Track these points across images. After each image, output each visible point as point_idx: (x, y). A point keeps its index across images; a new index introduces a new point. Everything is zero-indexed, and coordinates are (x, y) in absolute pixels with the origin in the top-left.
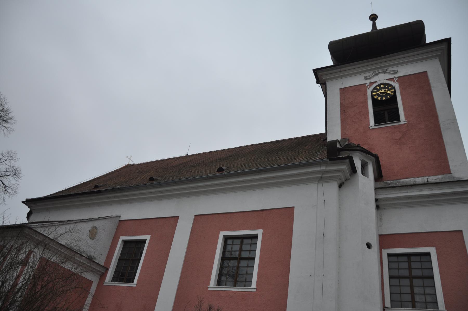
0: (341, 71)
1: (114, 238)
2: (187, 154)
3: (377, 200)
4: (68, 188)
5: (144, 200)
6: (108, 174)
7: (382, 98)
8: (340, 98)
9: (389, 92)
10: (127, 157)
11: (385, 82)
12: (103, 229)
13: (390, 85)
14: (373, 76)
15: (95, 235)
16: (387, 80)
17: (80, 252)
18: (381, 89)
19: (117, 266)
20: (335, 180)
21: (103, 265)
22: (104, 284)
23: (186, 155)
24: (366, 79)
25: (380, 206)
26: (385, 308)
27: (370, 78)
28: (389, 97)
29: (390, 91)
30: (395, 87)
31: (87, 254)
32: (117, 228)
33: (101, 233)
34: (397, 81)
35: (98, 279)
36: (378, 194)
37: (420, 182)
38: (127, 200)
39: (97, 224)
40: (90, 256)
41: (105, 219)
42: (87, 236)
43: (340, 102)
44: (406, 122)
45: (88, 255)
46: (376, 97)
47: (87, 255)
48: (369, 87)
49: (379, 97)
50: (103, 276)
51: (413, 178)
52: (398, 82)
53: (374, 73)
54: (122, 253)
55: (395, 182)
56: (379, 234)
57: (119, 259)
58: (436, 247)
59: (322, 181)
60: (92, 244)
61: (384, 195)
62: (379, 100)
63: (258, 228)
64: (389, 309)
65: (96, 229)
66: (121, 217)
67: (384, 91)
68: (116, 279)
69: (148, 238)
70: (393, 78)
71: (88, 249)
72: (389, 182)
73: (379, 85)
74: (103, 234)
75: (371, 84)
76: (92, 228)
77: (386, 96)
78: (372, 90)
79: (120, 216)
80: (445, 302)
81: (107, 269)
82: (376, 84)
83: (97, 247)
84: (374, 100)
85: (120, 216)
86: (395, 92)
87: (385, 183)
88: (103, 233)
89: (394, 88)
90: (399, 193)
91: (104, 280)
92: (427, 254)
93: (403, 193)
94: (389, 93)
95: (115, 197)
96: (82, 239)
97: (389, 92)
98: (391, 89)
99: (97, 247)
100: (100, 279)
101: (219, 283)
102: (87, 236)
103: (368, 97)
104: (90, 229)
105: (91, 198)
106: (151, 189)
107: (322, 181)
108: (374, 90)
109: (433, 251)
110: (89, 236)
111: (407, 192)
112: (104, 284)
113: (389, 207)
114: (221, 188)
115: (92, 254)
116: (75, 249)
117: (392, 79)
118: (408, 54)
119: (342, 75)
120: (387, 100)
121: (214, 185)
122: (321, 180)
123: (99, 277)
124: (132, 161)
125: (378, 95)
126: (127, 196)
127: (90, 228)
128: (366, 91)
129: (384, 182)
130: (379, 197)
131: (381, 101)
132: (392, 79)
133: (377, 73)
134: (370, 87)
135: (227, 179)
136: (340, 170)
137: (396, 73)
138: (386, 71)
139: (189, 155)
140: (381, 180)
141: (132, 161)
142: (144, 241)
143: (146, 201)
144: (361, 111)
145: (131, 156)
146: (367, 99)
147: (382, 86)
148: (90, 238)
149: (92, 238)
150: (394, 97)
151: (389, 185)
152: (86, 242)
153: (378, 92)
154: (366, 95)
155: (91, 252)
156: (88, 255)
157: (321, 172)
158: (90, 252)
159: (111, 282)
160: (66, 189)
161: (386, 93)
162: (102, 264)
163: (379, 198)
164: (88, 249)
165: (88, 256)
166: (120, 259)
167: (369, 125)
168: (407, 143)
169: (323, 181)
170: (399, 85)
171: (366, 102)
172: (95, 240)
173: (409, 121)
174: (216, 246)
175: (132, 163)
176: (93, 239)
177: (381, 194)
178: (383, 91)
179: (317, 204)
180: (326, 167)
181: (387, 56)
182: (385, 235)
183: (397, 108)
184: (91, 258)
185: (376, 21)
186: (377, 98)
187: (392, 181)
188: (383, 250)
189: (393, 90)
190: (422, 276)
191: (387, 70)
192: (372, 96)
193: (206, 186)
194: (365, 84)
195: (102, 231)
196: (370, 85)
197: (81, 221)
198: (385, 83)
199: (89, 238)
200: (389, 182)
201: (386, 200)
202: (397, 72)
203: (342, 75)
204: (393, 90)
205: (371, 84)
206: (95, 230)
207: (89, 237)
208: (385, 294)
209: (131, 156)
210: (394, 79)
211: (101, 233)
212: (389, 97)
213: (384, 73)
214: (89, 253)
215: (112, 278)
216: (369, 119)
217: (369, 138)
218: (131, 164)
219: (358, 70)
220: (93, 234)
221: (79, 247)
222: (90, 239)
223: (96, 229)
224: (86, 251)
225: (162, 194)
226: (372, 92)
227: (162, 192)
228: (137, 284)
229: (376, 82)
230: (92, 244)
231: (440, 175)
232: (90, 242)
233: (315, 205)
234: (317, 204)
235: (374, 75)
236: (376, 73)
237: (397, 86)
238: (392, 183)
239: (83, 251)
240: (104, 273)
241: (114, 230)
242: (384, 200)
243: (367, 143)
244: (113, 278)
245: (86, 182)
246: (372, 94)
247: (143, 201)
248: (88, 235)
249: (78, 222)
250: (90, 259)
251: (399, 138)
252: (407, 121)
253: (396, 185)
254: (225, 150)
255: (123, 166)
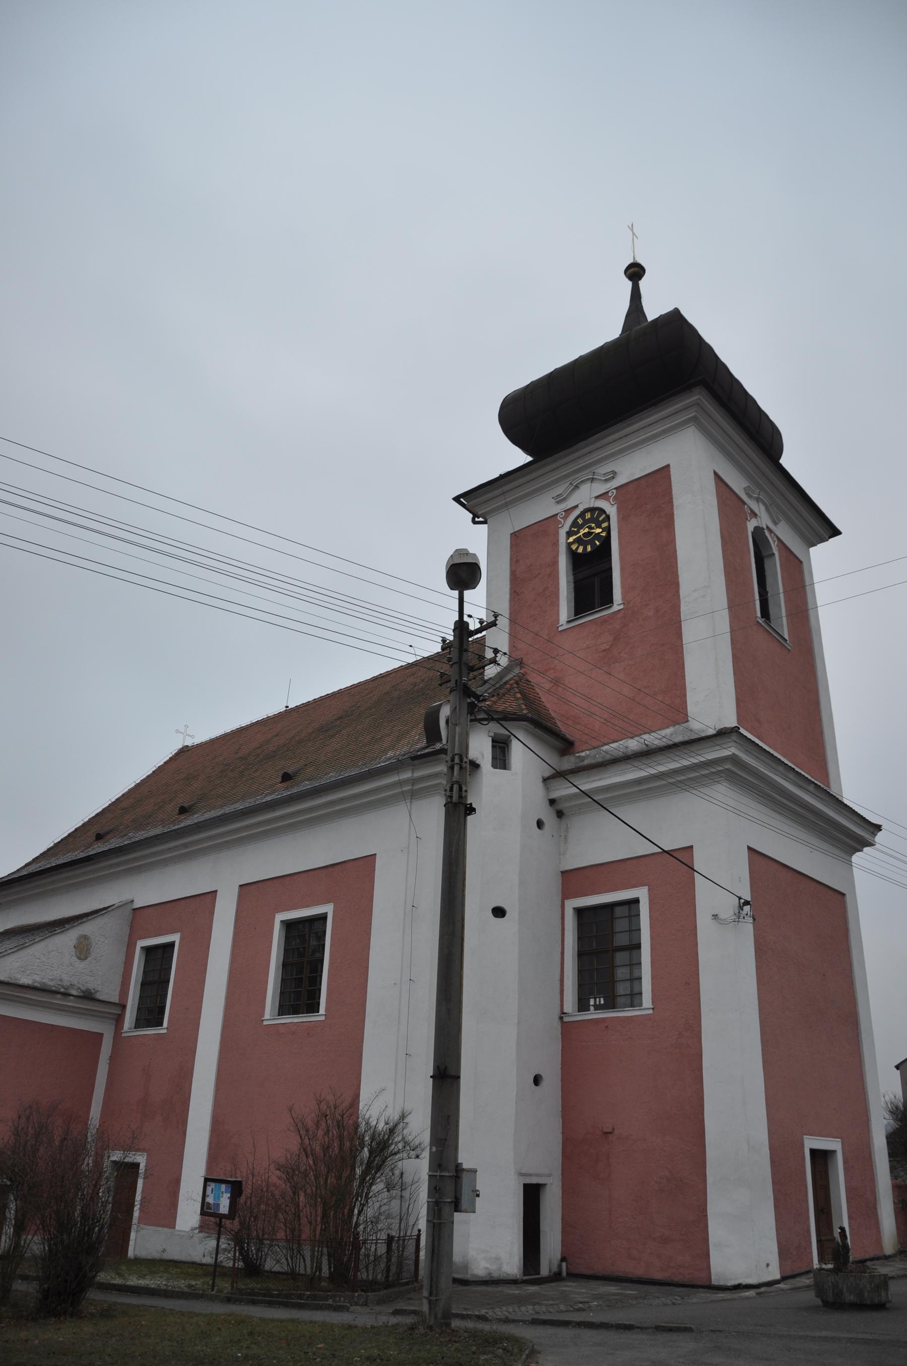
0: (503, 493)
1: (128, 945)
2: (287, 707)
3: (552, 802)
4: (59, 839)
5: (165, 863)
6: (138, 784)
7: (585, 549)
8: (511, 559)
9: (598, 530)
10: (177, 731)
11: (591, 506)
12: (102, 935)
13: (602, 511)
14: (570, 491)
15: (88, 949)
16: (597, 498)
17: (66, 989)
18: (580, 527)
19: (141, 998)
20: (435, 792)
21: (117, 1002)
22: (123, 1035)
23: (285, 709)
24: (558, 502)
25: (564, 812)
26: (562, 1015)
27: (564, 499)
28: (598, 543)
29: (600, 527)
30: (609, 515)
31: (79, 988)
32: (130, 924)
33: (100, 943)
34: (615, 498)
35: (113, 1027)
36: (553, 790)
37: (635, 748)
38: (139, 867)
39: (88, 928)
40: (87, 989)
41: (101, 915)
42: (71, 957)
43: (511, 570)
44: (622, 607)
45: (82, 988)
46: (574, 547)
47: (79, 990)
48: (562, 521)
49: (580, 547)
50: (119, 1020)
51: (623, 741)
52: (615, 502)
53: (571, 484)
54: (145, 972)
55: (593, 752)
56: (562, 870)
57: (142, 985)
58: (649, 886)
59: (405, 800)
60: (85, 969)
61: (563, 790)
62: (579, 554)
63: (328, 901)
64: (568, 1016)
65: (88, 939)
66: (135, 902)
67: (589, 529)
68: (140, 1023)
69: (175, 938)
70: (608, 492)
71: (80, 978)
72: (583, 754)
73: (582, 515)
74: (103, 944)
75: (568, 511)
76: (78, 939)
77: (592, 542)
78: (567, 530)
79: (133, 901)
80: (652, 991)
81: (124, 1007)
82: (576, 513)
83: (98, 971)
84: (574, 557)
85: (133, 901)
86: (608, 530)
87: (577, 756)
88: (103, 942)
89: (608, 518)
90: (587, 782)
91: (122, 1028)
92: (625, 902)
93: (594, 781)
94: (599, 533)
95: (118, 865)
96: (64, 964)
97: (598, 530)
98: (603, 521)
99: (97, 970)
100: (116, 1026)
101: (283, 1010)
102: (71, 957)
103: (560, 550)
104: (74, 942)
105: (83, 870)
106: (167, 842)
107: (405, 800)
108: (573, 529)
109: (642, 893)
110: (76, 955)
111: (600, 779)
112: (123, 1035)
113: (579, 811)
114: (271, 829)
115: (91, 986)
116: (54, 986)
117: (603, 496)
118: (631, 428)
119: (507, 500)
120: (596, 550)
121: (259, 824)
122: (414, 795)
123: (114, 1022)
124: (190, 736)
125: (579, 541)
126: (135, 859)
127: (75, 941)
128: (557, 534)
129: (574, 755)
130: (555, 795)
131: (585, 554)
132: (603, 496)
133: (577, 484)
134: (564, 522)
135: (274, 810)
136: (437, 774)
137: (613, 478)
138: (593, 475)
139: (290, 708)
140: (571, 751)
141: (190, 736)
142: (171, 945)
143: (168, 865)
144: (547, 588)
145: (187, 726)
146: (558, 555)
147: (588, 516)
148: (79, 958)
149: (82, 958)
150: (607, 541)
151: (583, 761)
152: (72, 968)
153: (579, 533)
154: (556, 544)
155: (86, 983)
156: (81, 990)
157: (414, 781)
158: (84, 984)
159: (135, 1028)
160: (55, 844)
161: (594, 532)
162: (115, 999)
163: (558, 797)
164: (80, 978)
165: (83, 992)
166: (144, 984)
167: (558, 620)
168: (620, 657)
169: (407, 801)
170: (618, 509)
171: (555, 563)
172: (89, 959)
173: (629, 603)
174: (271, 942)
175: (189, 742)
176: (86, 959)
177: (557, 789)
178: (587, 530)
179: (409, 846)
180: (413, 773)
181: (590, 439)
182: (571, 870)
183: (610, 569)
184: (91, 993)
185: (642, 283)
186: (577, 548)
187: (588, 752)
188: (566, 902)
189: (605, 525)
190: (630, 945)
191: (594, 473)
192: (569, 545)
193: (248, 827)
194: (557, 514)
195: (102, 939)
196: (565, 518)
197: (52, 933)
198: (593, 507)
199: (77, 960)
200: (583, 754)
201: (571, 799)
202: (614, 475)
203: (507, 500)
204: (605, 525)
205: (568, 511)
206: (85, 941)
207: (75, 958)
208: (565, 988)
209: (187, 726)
210: (610, 494)
211: (100, 943)
212: (598, 543)
213: (592, 482)
214: (83, 985)
215: (135, 1020)
216: (558, 605)
217: (556, 653)
218: (187, 746)
219: (541, 483)
220: (83, 950)
221: (61, 980)
222: (79, 961)
223: (88, 939)
224: (76, 984)
225: (187, 850)
226: (569, 534)
227: (185, 846)
228: (167, 1028)
229: (577, 506)
230: (85, 969)
231: (668, 728)
232: (80, 965)
233: (405, 848)
234: (409, 846)
235: (571, 489)
236: (574, 484)
237: (611, 510)
238: (588, 756)
239: (71, 985)
240: (120, 1014)
241: (127, 929)
242: (566, 800)
243: (553, 666)
244: (137, 1020)
245: (94, 817)
246: (609, 524)
247: (164, 866)
248: (73, 953)
249: (46, 938)
250: (88, 996)
251: (608, 647)
252: (624, 603)
253: (594, 759)
254: (340, 692)
255: (171, 755)
